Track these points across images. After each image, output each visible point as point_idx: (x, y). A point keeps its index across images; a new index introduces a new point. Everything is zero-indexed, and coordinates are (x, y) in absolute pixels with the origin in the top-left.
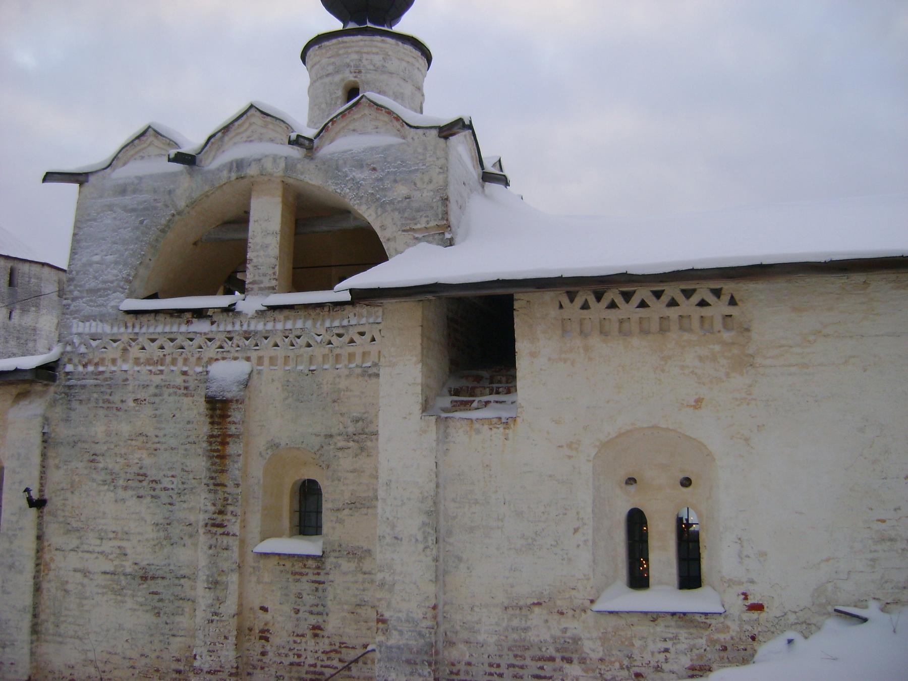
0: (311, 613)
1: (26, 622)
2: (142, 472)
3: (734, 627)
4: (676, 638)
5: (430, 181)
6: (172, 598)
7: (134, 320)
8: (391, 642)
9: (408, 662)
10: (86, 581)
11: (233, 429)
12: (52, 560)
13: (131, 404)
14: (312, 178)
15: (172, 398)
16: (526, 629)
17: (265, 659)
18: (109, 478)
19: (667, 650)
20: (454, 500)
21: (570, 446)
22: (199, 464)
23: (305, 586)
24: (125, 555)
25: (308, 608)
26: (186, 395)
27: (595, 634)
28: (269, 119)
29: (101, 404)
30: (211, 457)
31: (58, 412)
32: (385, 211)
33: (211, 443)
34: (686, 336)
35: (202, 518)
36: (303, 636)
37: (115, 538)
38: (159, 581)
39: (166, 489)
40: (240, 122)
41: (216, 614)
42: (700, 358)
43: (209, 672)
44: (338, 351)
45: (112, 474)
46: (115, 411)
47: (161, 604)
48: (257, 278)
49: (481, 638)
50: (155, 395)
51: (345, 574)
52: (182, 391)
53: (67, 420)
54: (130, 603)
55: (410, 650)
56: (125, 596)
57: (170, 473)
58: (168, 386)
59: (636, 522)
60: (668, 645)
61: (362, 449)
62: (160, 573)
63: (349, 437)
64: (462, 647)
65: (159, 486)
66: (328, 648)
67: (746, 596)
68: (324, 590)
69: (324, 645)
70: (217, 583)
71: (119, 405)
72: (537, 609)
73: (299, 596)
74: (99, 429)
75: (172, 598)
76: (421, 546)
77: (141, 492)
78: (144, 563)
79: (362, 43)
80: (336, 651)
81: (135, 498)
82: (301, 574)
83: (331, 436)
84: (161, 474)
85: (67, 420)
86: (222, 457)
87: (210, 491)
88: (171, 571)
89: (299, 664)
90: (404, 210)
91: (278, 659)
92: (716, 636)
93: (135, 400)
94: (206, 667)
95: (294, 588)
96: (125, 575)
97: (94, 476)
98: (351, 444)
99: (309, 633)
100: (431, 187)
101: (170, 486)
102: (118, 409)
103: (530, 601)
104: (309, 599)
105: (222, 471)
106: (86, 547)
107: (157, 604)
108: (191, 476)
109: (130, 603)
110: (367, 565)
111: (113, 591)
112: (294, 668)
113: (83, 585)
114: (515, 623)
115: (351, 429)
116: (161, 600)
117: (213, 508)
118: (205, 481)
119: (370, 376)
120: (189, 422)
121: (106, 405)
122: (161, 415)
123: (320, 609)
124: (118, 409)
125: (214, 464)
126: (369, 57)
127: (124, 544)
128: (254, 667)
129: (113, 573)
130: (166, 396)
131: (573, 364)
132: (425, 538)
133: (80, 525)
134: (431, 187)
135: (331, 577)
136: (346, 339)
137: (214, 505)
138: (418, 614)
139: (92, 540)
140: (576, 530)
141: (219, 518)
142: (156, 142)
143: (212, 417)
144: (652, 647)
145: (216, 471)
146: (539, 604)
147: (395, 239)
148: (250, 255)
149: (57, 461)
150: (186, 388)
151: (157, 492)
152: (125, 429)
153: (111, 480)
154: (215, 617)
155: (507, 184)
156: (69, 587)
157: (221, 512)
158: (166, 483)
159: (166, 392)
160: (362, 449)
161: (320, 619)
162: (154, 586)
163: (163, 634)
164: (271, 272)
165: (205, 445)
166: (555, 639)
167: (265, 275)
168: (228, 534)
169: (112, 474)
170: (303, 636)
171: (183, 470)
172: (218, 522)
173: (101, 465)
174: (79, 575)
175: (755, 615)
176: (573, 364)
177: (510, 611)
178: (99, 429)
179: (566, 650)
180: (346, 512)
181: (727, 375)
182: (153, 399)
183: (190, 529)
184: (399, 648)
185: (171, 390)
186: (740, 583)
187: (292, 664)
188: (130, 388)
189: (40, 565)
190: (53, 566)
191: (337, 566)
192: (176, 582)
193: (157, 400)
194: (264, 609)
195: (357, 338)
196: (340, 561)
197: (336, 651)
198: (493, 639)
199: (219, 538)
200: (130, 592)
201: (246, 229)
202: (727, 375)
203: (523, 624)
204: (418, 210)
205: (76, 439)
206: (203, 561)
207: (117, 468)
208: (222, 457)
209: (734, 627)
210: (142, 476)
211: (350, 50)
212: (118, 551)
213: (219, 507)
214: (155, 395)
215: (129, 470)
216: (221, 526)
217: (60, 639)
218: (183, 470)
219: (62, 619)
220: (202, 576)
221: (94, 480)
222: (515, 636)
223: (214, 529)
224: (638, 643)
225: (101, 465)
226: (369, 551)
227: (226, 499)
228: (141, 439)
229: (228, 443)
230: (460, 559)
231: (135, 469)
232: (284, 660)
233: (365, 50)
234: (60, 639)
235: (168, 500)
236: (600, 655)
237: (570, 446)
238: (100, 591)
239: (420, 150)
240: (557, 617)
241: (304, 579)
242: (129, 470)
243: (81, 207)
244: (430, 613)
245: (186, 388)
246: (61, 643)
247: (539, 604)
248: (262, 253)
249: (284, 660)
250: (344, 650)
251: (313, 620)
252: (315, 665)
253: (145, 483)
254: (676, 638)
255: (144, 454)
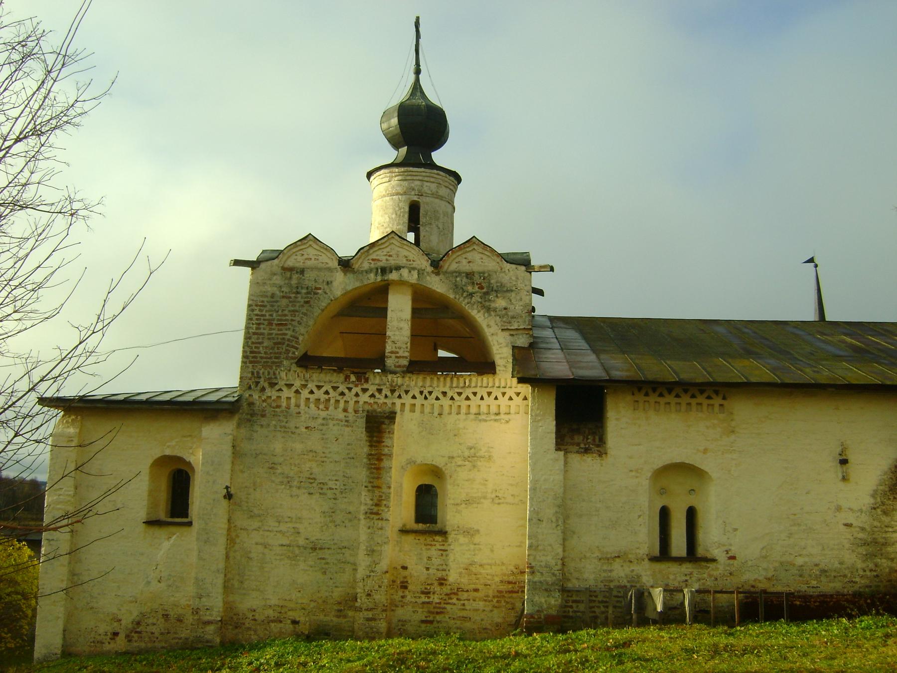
0: (438, 570)
1: (220, 581)
2: (312, 477)
3: (721, 568)
4: (691, 573)
5: (521, 299)
6: (335, 562)
7: (304, 372)
8: (536, 579)
9: (546, 590)
10: (266, 551)
11: (386, 451)
12: (237, 536)
13: (304, 430)
14: (437, 285)
15: (336, 428)
16: (611, 571)
17: (404, 600)
18: (286, 480)
19: (686, 581)
20: (571, 499)
21: (637, 471)
22: (361, 474)
23: (433, 552)
24: (299, 533)
25: (435, 567)
26: (347, 426)
27: (648, 573)
28: (405, 242)
29: (279, 429)
30: (369, 469)
31: (243, 432)
32: (490, 315)
33: (370, 460)
34: (700, 415)
35: (363, 508)
36: (432, 584)
37: (291, 522)
38: (326, 550)
39: (331, 489)
40: (383, 241)
41: (373, 571)
42: (707, 427)
43: (367, 610)
44: (459, 403)
45: (287, 477)
46: (290, 434)
47: (327, 566)
48: (394, 349)
49: (586, 576)
50: (323, 425)
51: (461, 545)
52: (344, 423)
53: (250, 439)
54: (302, 565)
55: (547, 583)
56: (299, 560)
57: (334, 478)
58: (333, 419)
59: (665, 514)
60: (688, 578)
61: (474, 466)
62: (327, 546)
63: (465, 459)
64: (574, 581)
65: (326, 487)
66: (449, 592)
67: (727, 552)
68: (447, 556)
69: (446, 589)
70: (373, 551)
71: (294, 430)
72: (617, 560)
73: (429, 558)
74: (278, 446)
75: (335, 562)
76: (554, 525)
77: (312, 491)
78: (313, 539)
79: (424, 174)
80: (454, 594)
81: (307, 495)
82: (431, 545)
83: (453, 458)
84: (328, 478)
85: (250, 439)
86: (378, 469)
87: (369, 491)
88: (335, 544)
89: (428, 603)
90: (503, 317)
91: (413, 600)
92: (712, 573)
93: (306, 428)
94: (364, 607)
95: (425, 554)
96: (299, 546)
97: (273, 479)
98: (467, 463)
99: (436, 583)
100: (521, 303)
101: (334, 487)
102: (293, 433)
103: (613, 555)
104: (436, 561)
105: (378, 478)
106: (266, 528)
107: (324, 566)
108: (350, 481)
109: (302, 565)
110: (477, 539)
111: (289, 557)
112: (425, 606)
113: (263, 554)
114: (605, 568)
115: (467, 454)
116: (327, 563)
117: (371, 502)
118: (365, 484)
119: (480, 420)
120: (348, 444)
121: (282, 430)
122: (327, 439)
123: (444, 567)
124: (293, 433)
125: (371, 473)
126: (428, 184)
127: (297, 525)
128: (397, 606)
129: (289, 546)
130: (331, 426)
131: (639, 426)
132: (557, 520)
133: (261, 512)
134: (521, 303)
135: (452, 547)
136: (464, 396)
137: (372, 500)
138: (553, 562)
139: (272, 523)
140: (639, 516)
141: (375, 509)
142: (315, 246)
143: (370, 441)
144: (679, 579)
145: (373, 478)
146: (619, 557)
147: (497, 334)
148: (388, 333)
149: (242, 467)
150: (347, 421)
151: (324, 491)
152: (299, 447)
153: (288, 481)
154: (372, 574)
155: (543, 295)
156: (253, 555)
157: (377, 505)
158: (331, 484)
159: (331, 423)
160: (474, 466)
161: (444, 573)
162: (321, 554)
163: (328, 586)
164: (404, 346)
165: (365, 460)
166: (627, 576)
167: (400, 348)
168: (382, 519)
169: (287, 477)
170: (432, 584)
171: (344, 476)
172: (375, 511)
173: (279, 471)
174: (260, 548)
175: (731, 562)
176: (639, 426)
177: (602, 561)
178: (278, 446)
179: (633, 581)
180: (463, 505)
181: (721, 437)
182: (320, 427)
183: (350, 516)
184: (541, 582)
185: (335, 422)
186: (724, 545)
187: (423, 603)
188: (303, 419)
189: (231, 541)
190: (238, 541)
191: (456, 540)
192: (339, 551)
193: (324, 428)
194: (404, 568)
195: (471, 396)
196: (458, 536)
197: (454, 594)
198: (592, 577)
199: (376, 522)
200: (302, 559)
201: (385, 316)
202: (721, 437)
203: (609, 568)
204: (513, 317)
205: (258, 452)
206: (363, 537)
207: (291, 474)
208: (378, 469)
209: (721, 568)
210: (312, 479)
211: (415, 178)
212: (292, 530)
213: (375, 501)
214: (323, 425)
215: (302, 475)
216: (377, 514)
217: (244, 592)
218: (344, 476)
219: (246, 577)
220: (363, 547)
221: (273, 482)
222: (605, 574)
223: (372, 516)
224: (672, 577)
225: (279, 471)
226: (478, 531)
227: (381, 496)
228: (311, 454)
229: (382, 460)
230: (574, 533)
231: (307, 475)
232: (418, 600)
233: (426, 179)
234: (244, 592)
235: (333, 496)
236: (651, 584)
237: (637, 471)
238: (278, 558)
239: (514, 278)
240: (628, 564)
241: (433, 548)
242: (302, 475)
243: (254, 284)
244: (560, 562)
245: (347, 421)
246: (245, 594)
247: (619, 557)
248: (397, 333)
249: (418, 600)
250: (460, 593)
251: (439, 574)
252: (440, 603)
253: (314, 485)
254: (691, 573)
255: (314, 465)
